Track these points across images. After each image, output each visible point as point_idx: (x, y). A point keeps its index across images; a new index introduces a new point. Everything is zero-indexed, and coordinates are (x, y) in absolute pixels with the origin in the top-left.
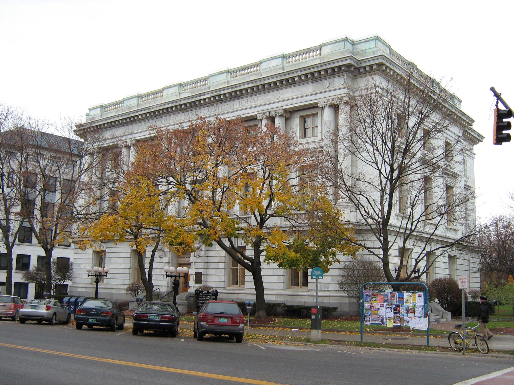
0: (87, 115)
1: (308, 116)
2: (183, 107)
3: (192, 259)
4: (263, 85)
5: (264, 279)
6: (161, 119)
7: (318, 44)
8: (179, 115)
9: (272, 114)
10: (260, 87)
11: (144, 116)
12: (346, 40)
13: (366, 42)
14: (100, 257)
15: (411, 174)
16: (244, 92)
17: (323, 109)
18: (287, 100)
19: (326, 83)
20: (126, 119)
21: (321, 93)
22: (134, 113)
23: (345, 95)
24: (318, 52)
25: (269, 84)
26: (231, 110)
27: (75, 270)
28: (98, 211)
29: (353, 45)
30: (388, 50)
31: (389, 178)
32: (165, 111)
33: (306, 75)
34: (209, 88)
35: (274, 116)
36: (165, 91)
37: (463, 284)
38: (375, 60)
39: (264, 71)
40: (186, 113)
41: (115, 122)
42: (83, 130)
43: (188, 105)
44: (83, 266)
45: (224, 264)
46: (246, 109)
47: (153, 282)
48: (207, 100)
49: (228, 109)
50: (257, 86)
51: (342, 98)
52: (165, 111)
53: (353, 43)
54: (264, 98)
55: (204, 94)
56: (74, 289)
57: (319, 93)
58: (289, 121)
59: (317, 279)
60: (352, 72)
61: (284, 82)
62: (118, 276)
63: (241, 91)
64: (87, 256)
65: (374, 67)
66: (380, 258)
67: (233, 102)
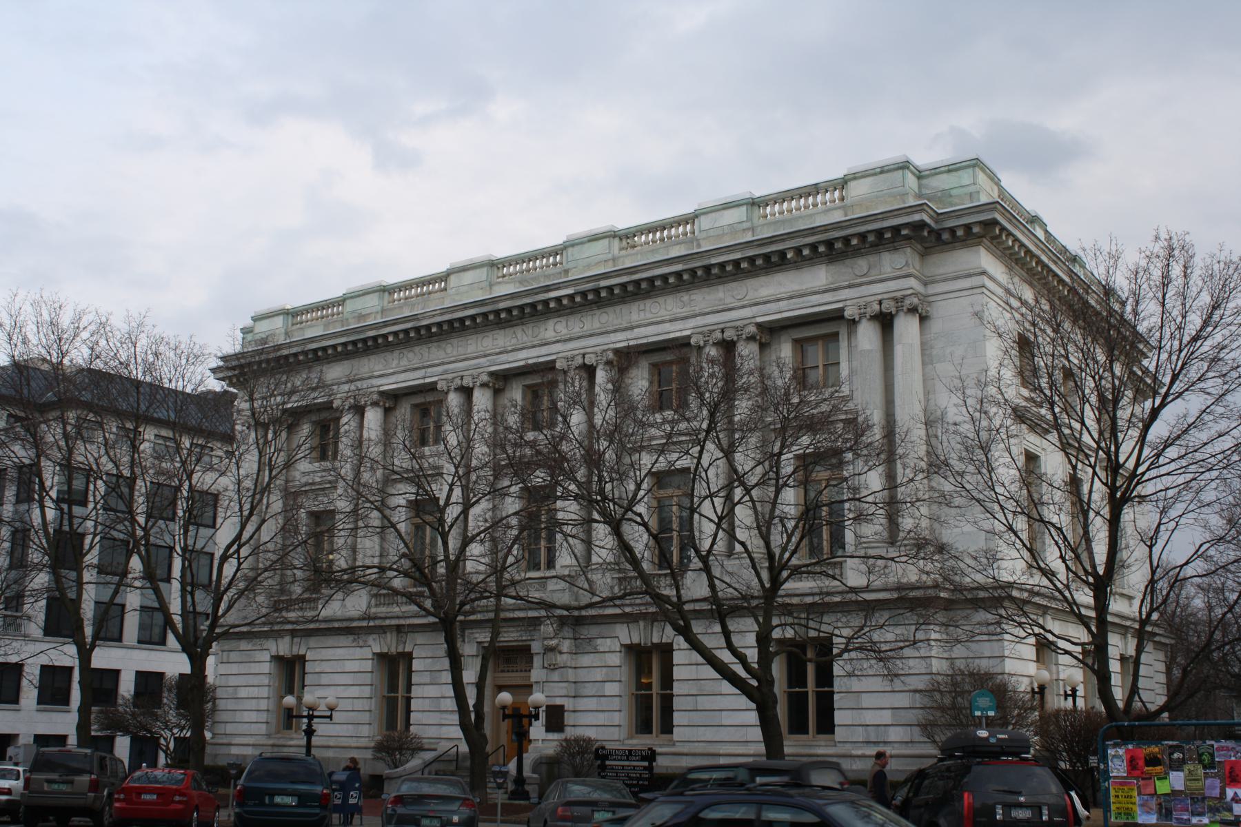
0: (245, 331)
4: (707, 268)
6: (443, 344)
7: (838, 173)
8: (490, 334)
10: (699, 273)
12: (905, 166)
13: (949, 171)
14: (291, 671)
15: (1168, 474)
17: (853, 323)
18: (764, 303)
19: (862, 264)
20: (354, 343)
21: (850, 286)
22: (376, 328)
24: (837, 193)
25: (722, 265)
26: (625, 325)
27: (221, 704)
28: (376, 561)
29: (919, 178)
32: (456, 325)
33: (814, 247)
34: (566, 271)
36: (453, 280)
39: (704, 235)
40: (509, 331)
41: (324, 349)
45: (617, 684)
49: (616, 322)
51: (904, 297)
52: (456, 325)
53: (920, 175)
54: (707, 297)
55: (557, 287)
56: (223, 750)
57: (844, 288)
60: (922, 240)
63: (651, 280)
64: (255, 668)
65: (976, 230)
67: (627, 306)
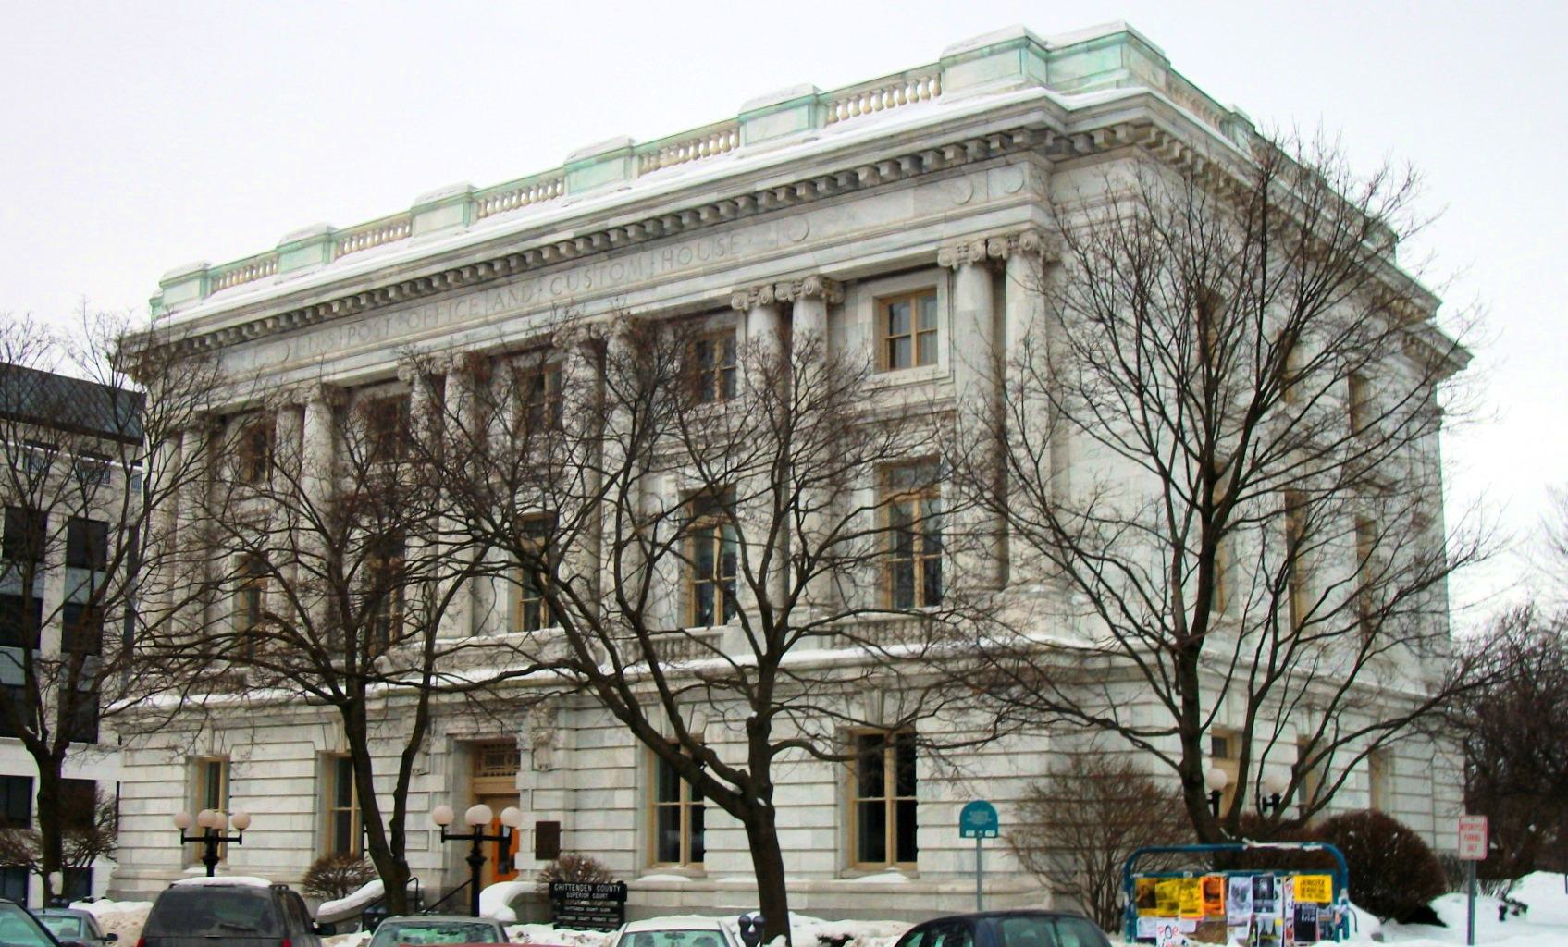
0: (155, 303)
1: (905, 297)
2: (482, 271)
3: (525, 778)
4: (753, 197)
5: (784, 840)
6: (406, 315)
8: (467, 298)
9: (783, 293)
10: (742, 203)
11: (349, 303)
12: (1027, 42)
13: (1089, 50)
14: (213, 779)
16: (685, 220)
17: (952, 272)
18: (831, 246)
20: (289, 316)
21: (947, 220)
22: (317, 295)
23: (1026, 226)
25: (772, 193)
26: (644, 280)
29: (1047, 61)
30: (1162, 75)
31: (1200, 501)
33: (895, 163)
35: (790, 298)
37: (1473, 843)
38: (1123, 110)
40: (493, 293)
41: (250, 325)
42: (151, 354)
43: (497, 267)
44: (153, 807)
46: (695, 276)
47: (409, 857)
48: (563, 250)
50: (733, 202)
52: (421, 286)
58: (840, 316)
59: (979, 838)
61: (822, 187)
62: (275, 840)
63: (676, 216)
65: (1121, 134)
66: (1172, 763)
